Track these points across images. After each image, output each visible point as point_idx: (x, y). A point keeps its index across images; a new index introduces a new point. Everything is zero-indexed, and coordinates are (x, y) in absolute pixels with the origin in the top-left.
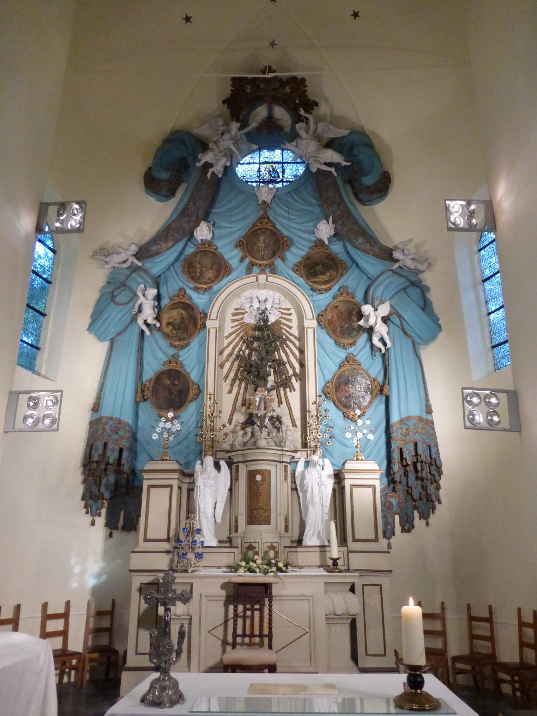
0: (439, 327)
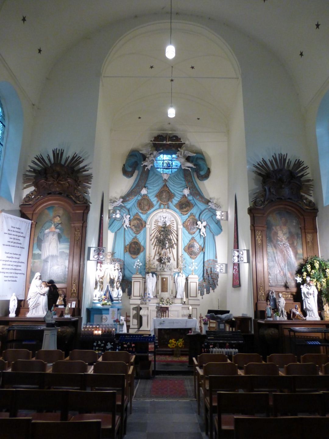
0: (222, 230)
